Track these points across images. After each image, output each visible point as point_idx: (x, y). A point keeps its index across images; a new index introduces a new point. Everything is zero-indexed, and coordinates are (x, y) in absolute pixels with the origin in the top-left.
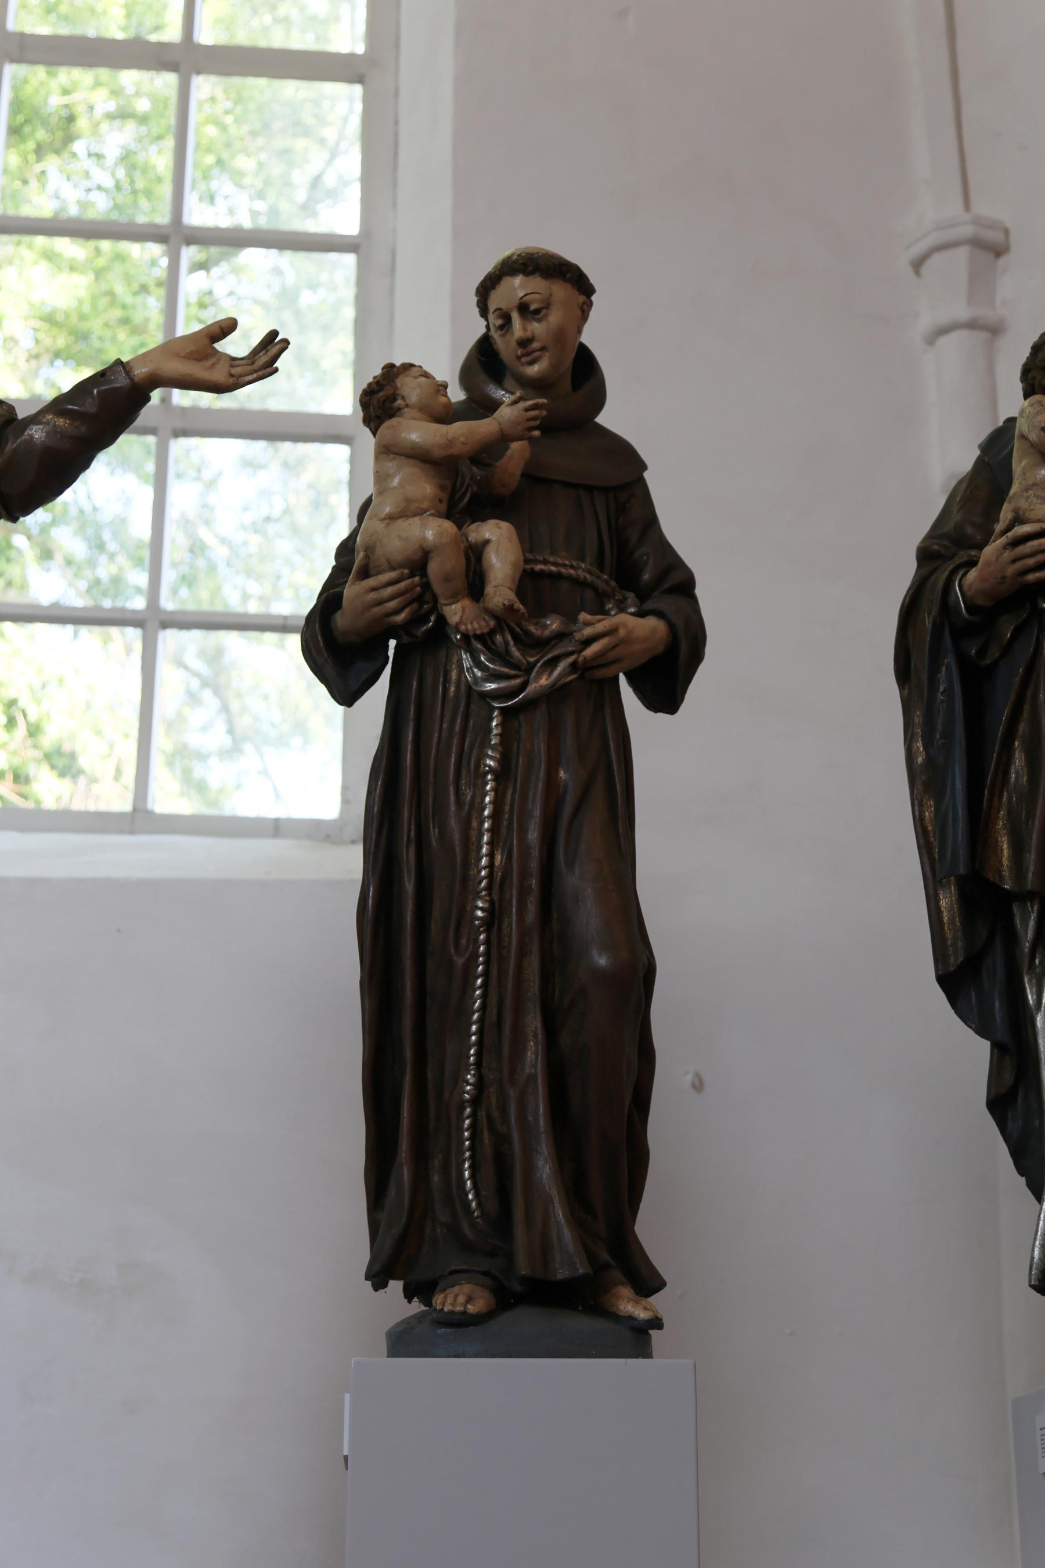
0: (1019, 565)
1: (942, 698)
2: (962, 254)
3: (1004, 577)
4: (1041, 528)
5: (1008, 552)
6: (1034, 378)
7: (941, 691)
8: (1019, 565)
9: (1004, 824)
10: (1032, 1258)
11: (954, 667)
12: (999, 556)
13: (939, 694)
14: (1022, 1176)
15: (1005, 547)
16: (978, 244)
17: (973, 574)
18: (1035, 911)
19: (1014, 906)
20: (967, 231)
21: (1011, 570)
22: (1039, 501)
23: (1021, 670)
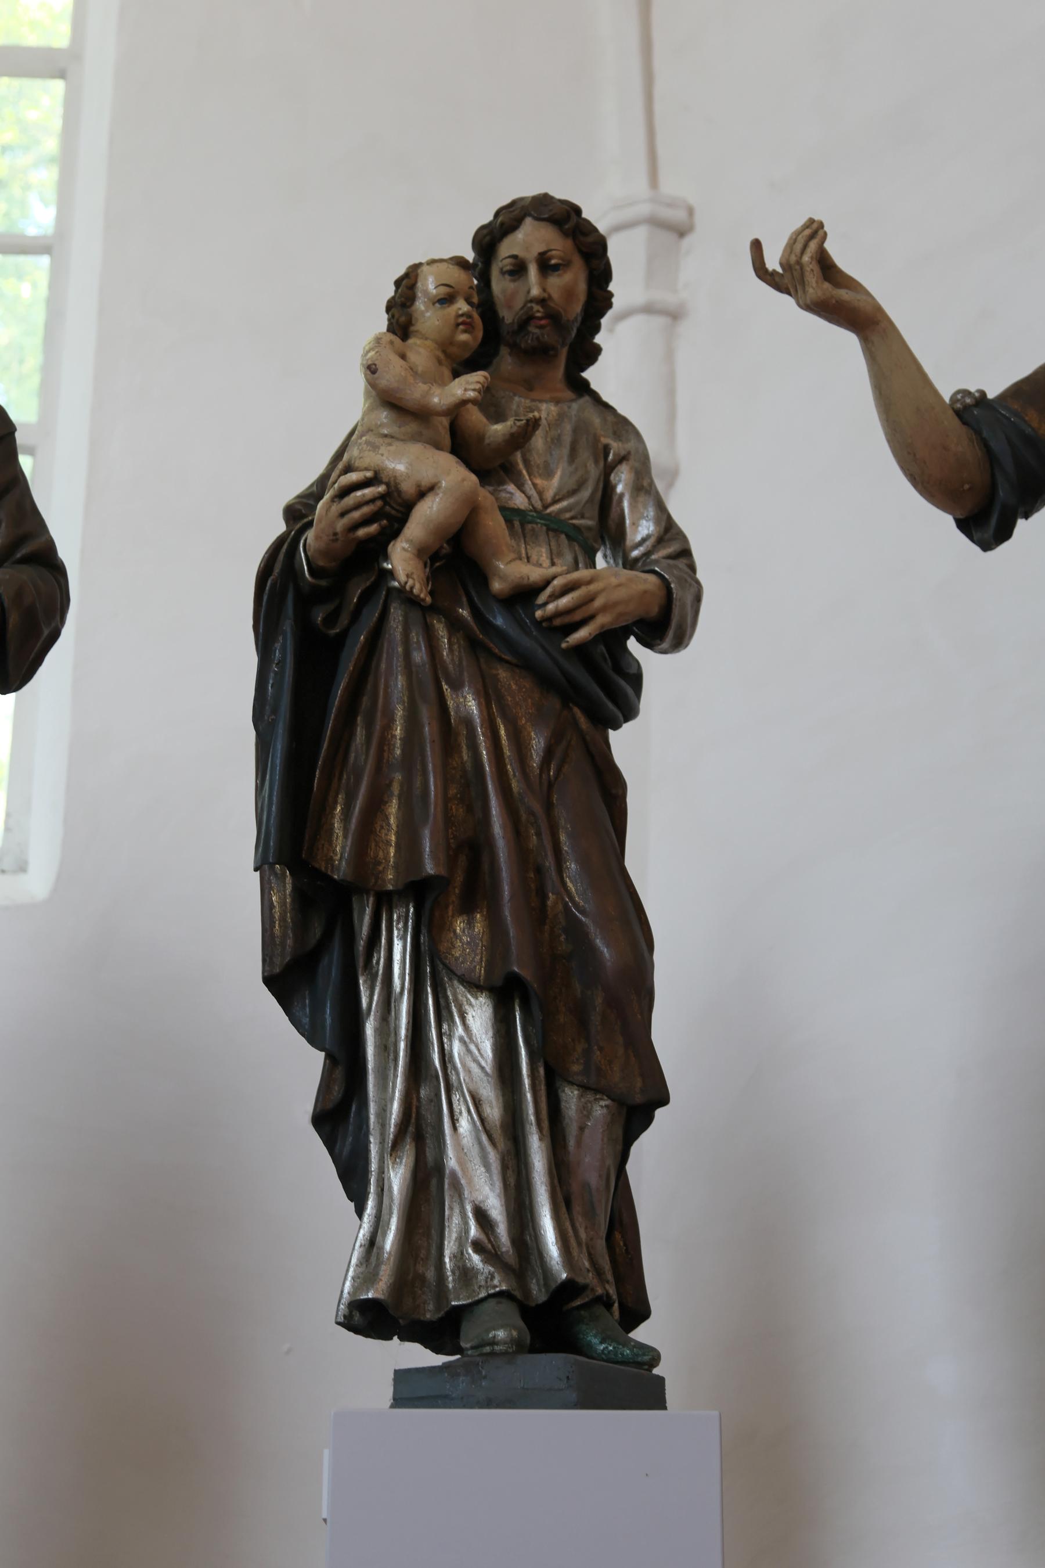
0: (346, 520)
1: (276, 669)
2: (641, 233)
4: (365, 477)
5: (335, 504)
7: (276, 662)
8: (346, 520)
9: (342, 808)
10: (342, 1292)
12: (328, 510)
13: (274, 665)
14: (352, 1201)
15: (333, 500)
16: (656, 223)
17: (310, 535)
18: (370, 905)
19: (354, 899)
20: (644, 209)
21: (341, 524)
23: (362, 637)
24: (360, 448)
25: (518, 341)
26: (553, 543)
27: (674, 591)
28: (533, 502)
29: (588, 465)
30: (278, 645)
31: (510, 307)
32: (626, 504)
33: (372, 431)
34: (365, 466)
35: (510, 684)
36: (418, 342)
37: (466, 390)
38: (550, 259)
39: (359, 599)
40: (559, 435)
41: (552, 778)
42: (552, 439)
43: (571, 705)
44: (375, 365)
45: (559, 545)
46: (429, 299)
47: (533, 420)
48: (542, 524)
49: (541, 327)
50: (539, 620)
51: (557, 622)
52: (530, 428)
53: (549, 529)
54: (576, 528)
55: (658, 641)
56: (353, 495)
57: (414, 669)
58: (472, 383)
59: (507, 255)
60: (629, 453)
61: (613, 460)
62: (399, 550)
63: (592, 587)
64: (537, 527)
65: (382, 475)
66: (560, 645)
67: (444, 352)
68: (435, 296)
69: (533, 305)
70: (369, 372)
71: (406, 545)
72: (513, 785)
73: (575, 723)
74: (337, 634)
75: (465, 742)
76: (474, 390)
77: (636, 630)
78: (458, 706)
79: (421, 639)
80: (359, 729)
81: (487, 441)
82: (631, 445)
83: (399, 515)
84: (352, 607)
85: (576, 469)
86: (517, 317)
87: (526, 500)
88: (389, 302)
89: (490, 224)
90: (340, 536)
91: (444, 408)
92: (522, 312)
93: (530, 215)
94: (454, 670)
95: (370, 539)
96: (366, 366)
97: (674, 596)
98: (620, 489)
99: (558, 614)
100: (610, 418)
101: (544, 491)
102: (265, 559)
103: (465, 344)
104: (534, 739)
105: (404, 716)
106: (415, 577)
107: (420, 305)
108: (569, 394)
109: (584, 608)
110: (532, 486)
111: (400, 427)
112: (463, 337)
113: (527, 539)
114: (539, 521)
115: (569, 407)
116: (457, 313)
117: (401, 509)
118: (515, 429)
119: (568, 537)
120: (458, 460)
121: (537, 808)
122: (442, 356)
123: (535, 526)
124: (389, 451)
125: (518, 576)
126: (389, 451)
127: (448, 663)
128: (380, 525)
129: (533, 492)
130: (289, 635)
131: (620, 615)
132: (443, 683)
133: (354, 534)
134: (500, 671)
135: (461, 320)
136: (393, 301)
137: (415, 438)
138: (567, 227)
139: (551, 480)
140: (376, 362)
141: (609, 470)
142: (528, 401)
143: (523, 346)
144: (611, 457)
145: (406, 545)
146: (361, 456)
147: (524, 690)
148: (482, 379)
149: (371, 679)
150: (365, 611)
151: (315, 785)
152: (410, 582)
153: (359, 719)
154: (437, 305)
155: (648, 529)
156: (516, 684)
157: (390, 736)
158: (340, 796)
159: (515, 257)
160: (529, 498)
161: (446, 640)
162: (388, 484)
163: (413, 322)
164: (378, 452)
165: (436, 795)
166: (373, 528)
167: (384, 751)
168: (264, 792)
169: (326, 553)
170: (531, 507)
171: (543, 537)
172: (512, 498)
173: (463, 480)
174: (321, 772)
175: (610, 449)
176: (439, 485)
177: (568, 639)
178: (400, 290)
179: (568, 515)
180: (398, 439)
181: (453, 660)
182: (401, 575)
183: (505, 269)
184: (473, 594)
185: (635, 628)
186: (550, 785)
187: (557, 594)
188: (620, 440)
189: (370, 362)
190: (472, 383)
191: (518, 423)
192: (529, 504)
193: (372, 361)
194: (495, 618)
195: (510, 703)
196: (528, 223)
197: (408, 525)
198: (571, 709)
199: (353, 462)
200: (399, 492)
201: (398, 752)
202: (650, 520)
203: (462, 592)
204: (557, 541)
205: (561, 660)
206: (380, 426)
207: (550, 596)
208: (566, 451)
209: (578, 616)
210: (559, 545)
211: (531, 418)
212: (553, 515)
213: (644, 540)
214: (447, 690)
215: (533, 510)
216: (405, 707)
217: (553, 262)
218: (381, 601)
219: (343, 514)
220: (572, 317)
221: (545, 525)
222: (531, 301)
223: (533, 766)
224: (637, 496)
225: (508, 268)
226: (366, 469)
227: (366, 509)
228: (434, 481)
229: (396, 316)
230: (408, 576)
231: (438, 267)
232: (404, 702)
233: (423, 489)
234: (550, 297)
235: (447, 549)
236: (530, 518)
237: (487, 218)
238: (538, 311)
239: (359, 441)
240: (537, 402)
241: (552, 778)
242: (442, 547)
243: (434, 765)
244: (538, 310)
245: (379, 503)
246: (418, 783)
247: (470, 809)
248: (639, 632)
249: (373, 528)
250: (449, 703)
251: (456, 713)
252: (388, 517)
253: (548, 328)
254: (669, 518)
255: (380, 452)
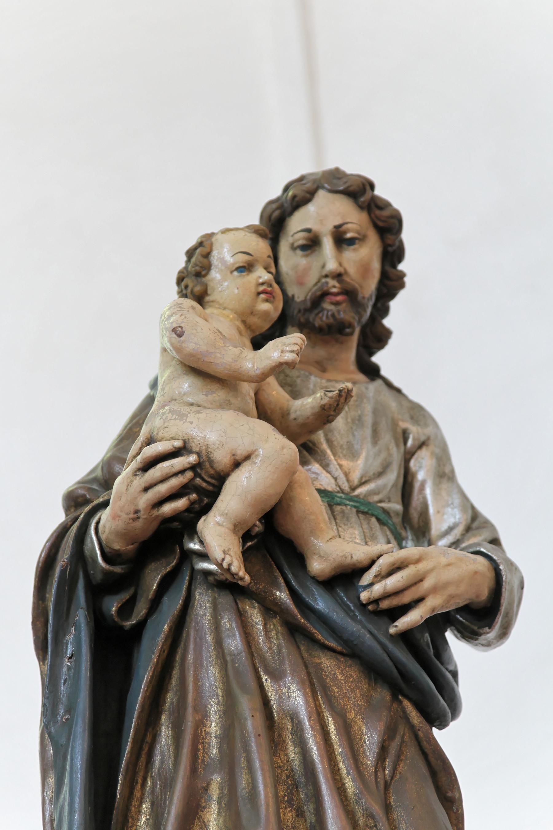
1: (69, 664)
3: (137, 512)
5: (138, 478)
6: (186, 287)
9: (147, 819)
11: (83, 625)
13: (67, 660)
17: (105, 515)
22: (174, 416)
23: (166, 627)
24: (164, 417)
25: (311, 320)
26: (365, 526)
27: (503, 573)
28: (340, 483)
29: (391, 447)
30: (70, 638)
31: (300, 283)
32: (428, 491)
33: (175, 400)
34: (173, 435)
35: (335, 674)
36: (216, 311)
37: (282, 352)
38: (345, 232)
39: (159, 585)
40: (360, 416)
41: (388, 778)
42: (353, 421)
43: (400, 697)
44: (182, 328)
45: (371, 529)
46: (226, 267)
47: (346, 390)
48: (352, 506)
49: (337, 304)
50: (364, 602)
51: (385, 605)
52: (342, 400)
53: (358, 512)
54: (386, 512)
55: (487, 629)
56: (159, 466)
57: (228, 658)
58: (289, 345)
59: (299, 229)
60: (428, 438)
61: (413, 445)
62: (212, 525)
63: (422, 567)
64: (347, 509)
65: (193, 445)
66: (387, 630)
67: (244, 322)
68: (233, 264)
69: (329, 280)
70: (174, 335)
71: (218, 519)
72: (347, 785)
73: (406, 717)
74: (134, 627)
75: (291, 737)
76: (292, 351)
77: (461, 619)
78: (280, 698)
79: (234, 625)
80: (163, 729)
81: (292, 416)
82: (429, 431)
83: (210, 488)
84: (151, 594)
85: (380, 452)
86: (310, 294)
87: (333, 481)
88: (180, 272)
89: (278, 200)
90: (141, 514)
91: (258, 372)
92: (316, 288)
93: (323, 188)
94: (273, 658)
95: (176, 517)
96: (171, 329)
97: (504, 579)
98: (421, 476)
99: (387, 596)
100: (405, 403)
101: (349, 473)
102: (46, 549)
103: (266, 314)
104: (366, 735)
105: (219, 711)
106: (232, 553)
107: (215, 275)
108: (361, 377)
109: (413, 589)
110: (338, 467)
111: (206, 395)
112: (265, 306)
113: (337, 521)
114: (348, 502)
115: (367, 388)
116: (257, 281)
117: (213, 481)
118: (326, 401)
119: (378, 520)
120: (273, 428)
121: (377, 810)
122: (242, 327)
123: (344, 508)
124: (199, 419)
125: (341, 554)
126: (199, 419)
127: (265, 651)
128: (189, 499)
129: (339, 473)
130: (83, 626)
131: (452, 597)
132: (262, 674)
133: (158, 511)
134: (323, 660)
135: (261, 288)
136: (185, 272)
137: (224, 405)
138: (362, 199)
139: (357, 461)
140: (182, 325)
141: (408, 456)
142: (324, 381)
143: (317, 325)
144: (410, 443)
145: (218, 519)
146: (165, 425)
147: (351, 680)
148: (299, 342)
149: (176, 673)
150: (165, 600)
151: (118, 793)
152: (228, 559)
153: (163, 717)
154: (236, 273)
155: (455, 517)
156: (342, 674)
157: (203, 734)
158: (144, 806)
159: (309, 231)
160: (336, 479)
161: (261, 627)
162: (198, 454)
163: (209, 292)
164: (186, 420)
165: (266, 796)
166: (181, 504)
167: (198, 750)
168: (62, 797)
169: (124, 535)
170: (338, 489)
171: (354, 518)
172: (317, 478)
173: (283, 448)
174: (125, 778)
175: (409, 434)
176: (256, 453)
177: (396, 623)
178: (193, 260)
179: (376, 498)
180: (205, 407)
181: (270, 648)
182: (217, 553)
183: (296, 244)
184: (290, 576)
185: (458, 617)
186: (387, 786)
187: (383, 573)
188: (419, 425)
189: (175, 325)
190: (289, 345)
191: (330, 394)
192: (336, 485)
193: (176, 323)
194: (315, 600)
195: (337, 695)
196: (321, 195)
197: (221, 498)
198: (401, 702)
199: (155, 433)
200: (211, 462)
201: (215, 751)
202: (455, 507)
203: (277, 573)
204: (368, 523)
205: (391, 646)
206: (184, 394)
207: (376, 576)
208: (368, 431)
209: (406, 598)
210: (371, 529)
211: (344, 388)
212: (361, 497)
213: (451, 529)
214: (266, 680)
215: (341, 492)
216: (219, 702)
217: (349, 235)
218: (185, 587)
219: (146, 489)
220: (367, 295)
221: (355, 507)
222: (326, 276)
223: (367, 763)
224: (440, 483)
225: (301, 242)
226: (173, 438)
227: (175, 482)
228: (251, 448)
229: (191, 285)
230: (224, 552)
231: (234, 234)
232: (218, 695)
233: (238, 458)
234: (346, 272)
235: (259, 528)
236: (338, 499)
237: (276, 192)
238: (334, 287)
239: (161, 411)
240: (334, 382)
241: (388, 778)
242: (255, 525)
243: (261, 761)
244: (333, 285)
245: (189, 475)
246: (243, 782)
247: (300, 813)
248: (464, 621)
249: (181, 504)
250: (270, 694)
251: (279, 705)
252: (198, 490)
253: (344, 305)
254: (473, 508)
255: (188, 420)
